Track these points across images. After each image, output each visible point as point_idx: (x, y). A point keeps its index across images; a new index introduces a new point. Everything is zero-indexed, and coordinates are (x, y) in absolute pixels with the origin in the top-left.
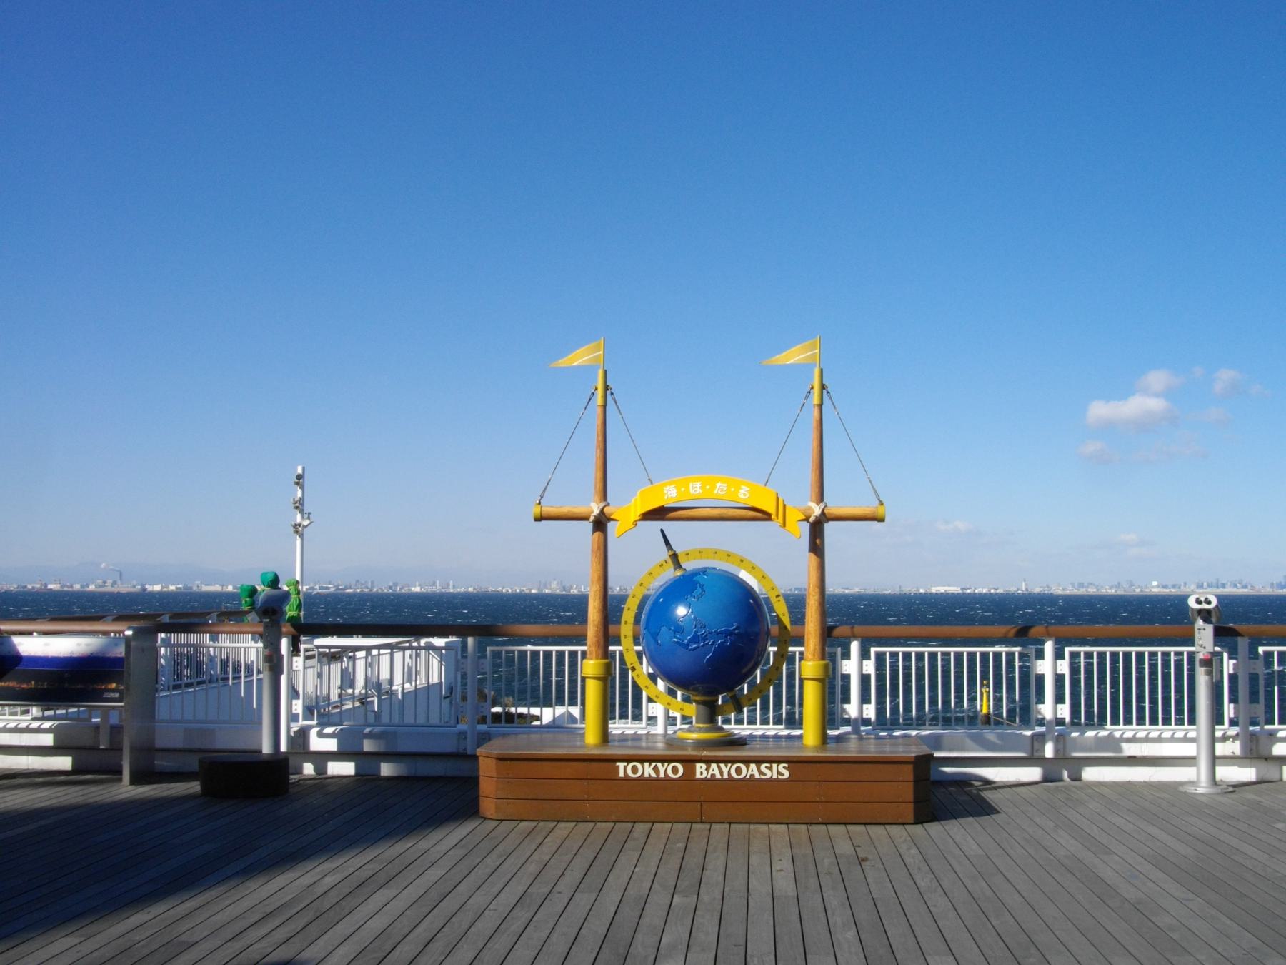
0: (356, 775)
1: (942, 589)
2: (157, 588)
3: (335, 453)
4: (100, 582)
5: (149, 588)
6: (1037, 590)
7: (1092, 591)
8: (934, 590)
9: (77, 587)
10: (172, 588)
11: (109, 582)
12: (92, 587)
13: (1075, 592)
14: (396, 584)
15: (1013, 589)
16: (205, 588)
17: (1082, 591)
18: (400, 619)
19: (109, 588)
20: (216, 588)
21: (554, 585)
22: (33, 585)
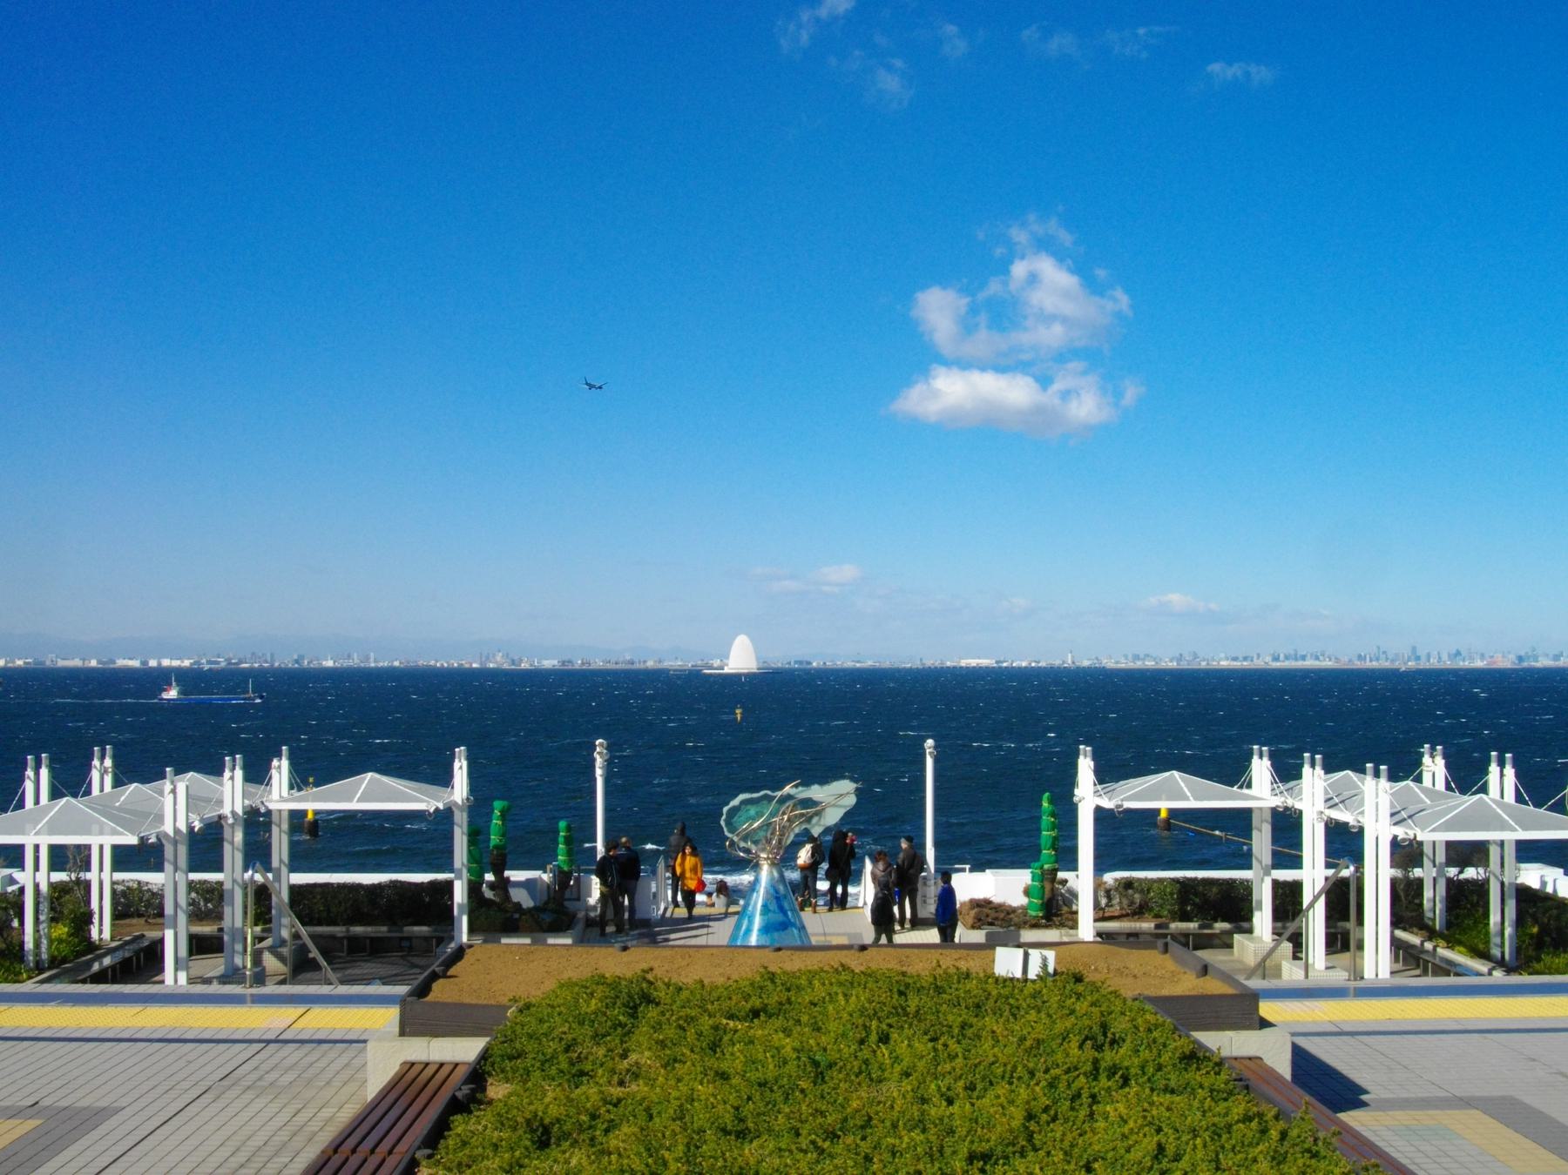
1: (973, 662)
6: (1086, 663)
7: (1150, 664)
8: (963, 663)
10: (20, 663)
13: (1131, 665)
14: (302, 657)
15: (1057, 663)
16: (61, 663)
17: (1139, 665)
20: (76, 663)
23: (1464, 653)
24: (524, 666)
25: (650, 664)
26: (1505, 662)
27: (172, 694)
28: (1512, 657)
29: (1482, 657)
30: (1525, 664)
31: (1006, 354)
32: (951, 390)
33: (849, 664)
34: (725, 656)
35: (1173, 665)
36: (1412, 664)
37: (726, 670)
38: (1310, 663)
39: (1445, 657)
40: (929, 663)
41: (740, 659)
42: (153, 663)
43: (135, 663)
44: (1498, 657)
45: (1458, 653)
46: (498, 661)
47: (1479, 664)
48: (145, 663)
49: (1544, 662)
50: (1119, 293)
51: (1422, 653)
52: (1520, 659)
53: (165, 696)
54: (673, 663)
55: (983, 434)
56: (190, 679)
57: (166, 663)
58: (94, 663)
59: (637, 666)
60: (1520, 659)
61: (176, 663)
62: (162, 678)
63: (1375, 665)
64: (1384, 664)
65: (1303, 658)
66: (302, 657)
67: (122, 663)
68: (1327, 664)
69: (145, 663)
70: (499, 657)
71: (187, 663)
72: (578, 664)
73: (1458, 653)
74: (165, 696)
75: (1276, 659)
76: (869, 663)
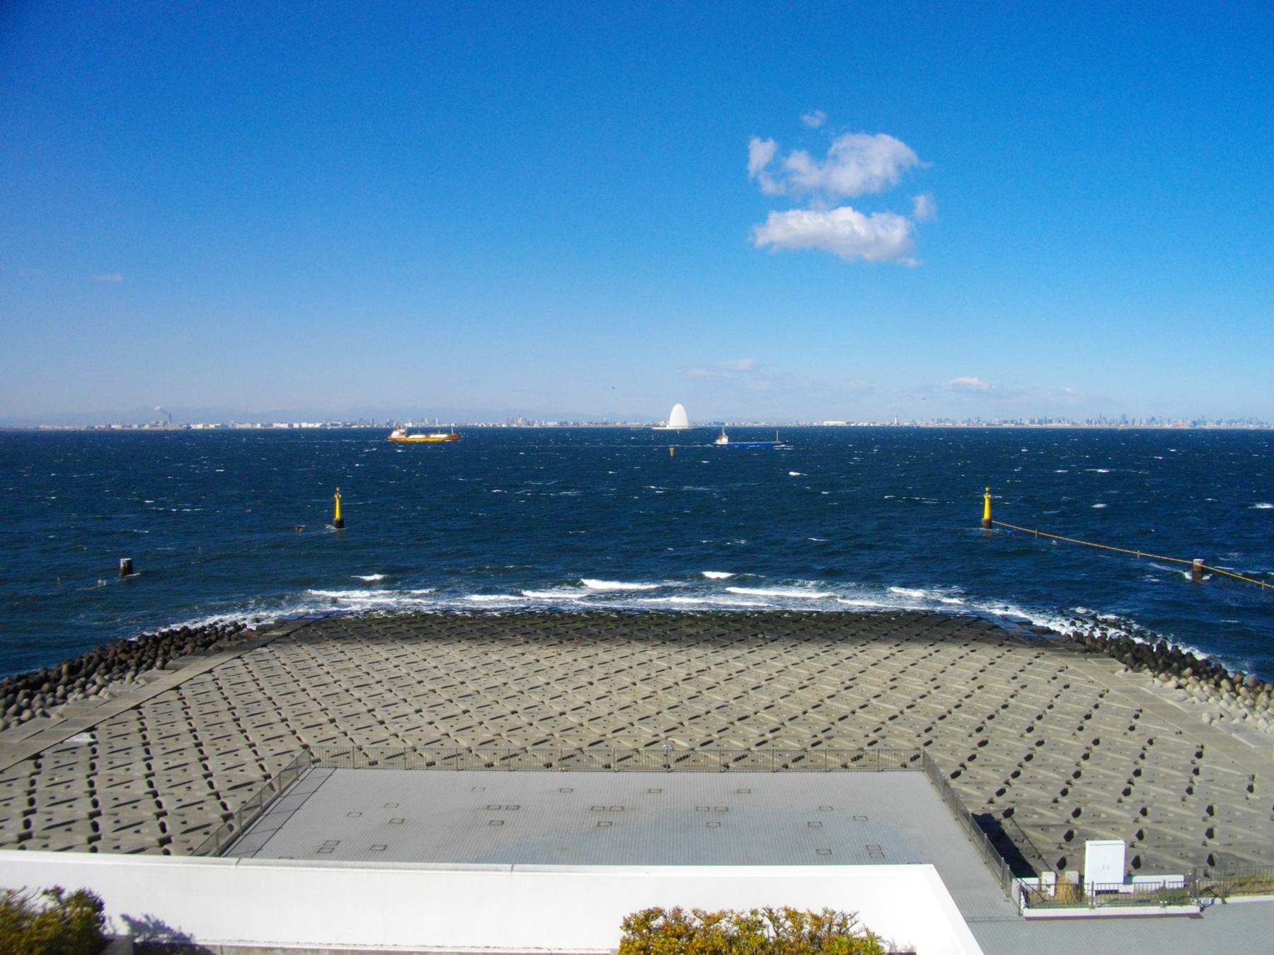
0: (100, 935)
1: (831, 423)
2: (200, 426)
3: (33, 875)
4: (153, 422)
5: (193, 427)
6: (907, 424)
7: (949, 425)
8: (825, 424)
9: (135, 427)
10: (212, 426)
11: (161, 423)
12: (147, 427)
13: (937, 425)
14: (392, 421)
15: (888, 423)
16: (238, 426)
17: (941, 425)
18: (443, 431)
19: (161, 427)
20: (247, 426)
21: (520, 421)
22: (100, 426)
23: (1157, 419)
24: (536, 426)
25: (618, 424)
26: (1185, 425)
27: (724, 441)
28: (1189, 422)
29: (1169, 421)
30: (1198, 427)
31: (842, 196)
32: (793, 226)
33: (749, 424)
34: (667, 419)
35: (965, 425)
36: (1122, 427)
37: (668, 428)
38: (1054, 425)
39: (1144, 421)
40: (802, 423)
41: (677, 420)
42: (296, 426)
43: (285, 426)
44: (1180, 422)
45: (1153, 419)
46: (519, 423)
47: (1167, 426)
48: (291, 425)
49: (1210, 426)
50: (818, 113)
51: (1109, 420)
52: (1195, 423)
53: (718, 442)
54: (633, 424)
55: (815, 260)
56: (733, 433)
57: (304, 425)
58: (259, 426)
59: (609, 426)
60: (1195, 423)
61: (311, 426)
62: (716, 433)
63: (1098, 426)
64: (1104, 426)
65: (1051, 421)
66: (392, 421)
67: (277, 425)
68: (1067, 425)
69: (291, 425)
70: (520, 421)
71: (318, 425)
72: (571, 424)
73: (1153, 419)
74: (718, 442)
75: (1032, 422)
76: (762, 424)
